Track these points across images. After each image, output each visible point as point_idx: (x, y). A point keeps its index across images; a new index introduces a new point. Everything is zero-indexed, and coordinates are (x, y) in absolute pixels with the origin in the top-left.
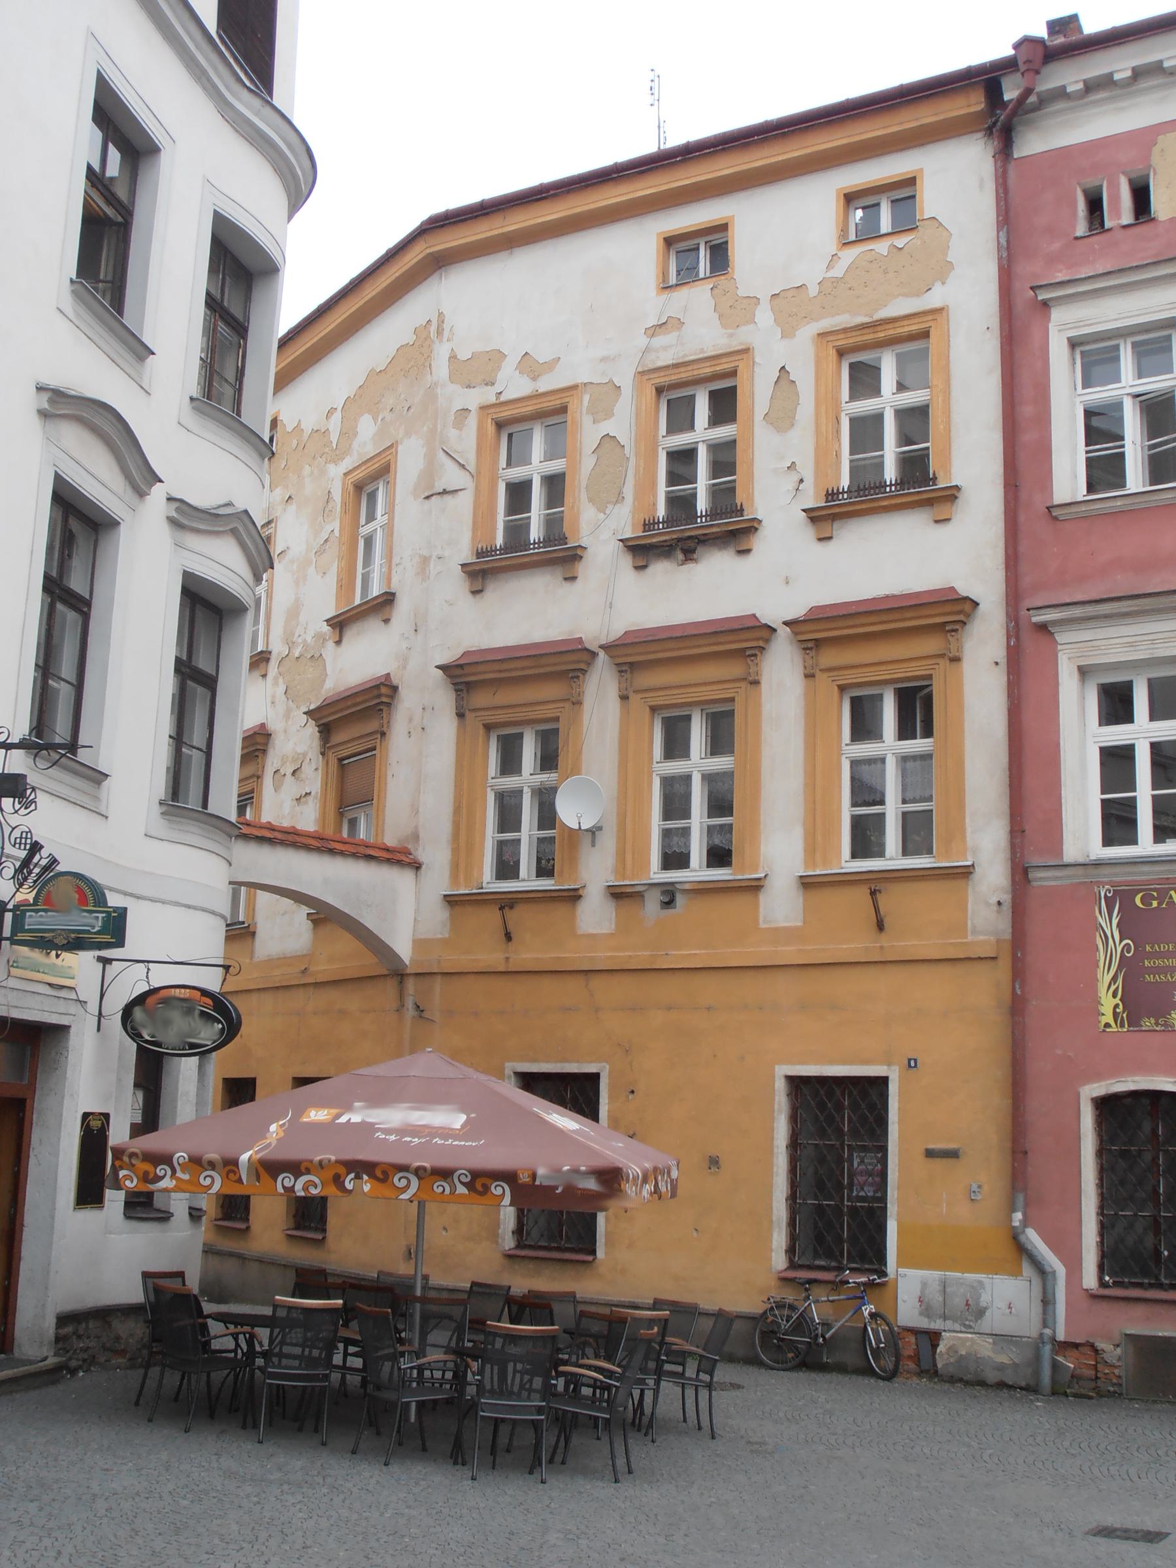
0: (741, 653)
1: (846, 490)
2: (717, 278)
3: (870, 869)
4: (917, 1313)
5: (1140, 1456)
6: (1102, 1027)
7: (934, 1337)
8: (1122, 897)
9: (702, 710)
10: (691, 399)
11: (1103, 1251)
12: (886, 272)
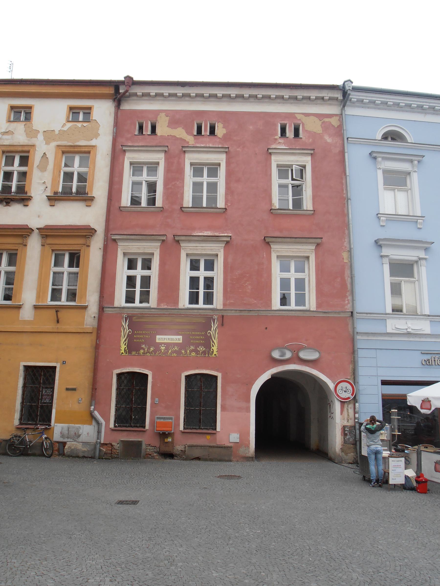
0: (21, 236)
1: (60, 192)
2: (27, 122)
3: (56, 304)
4: (60, 437)
5: (127, 476)
6: (121, 354)
7: (64, 444)
8: (130, 318)
9: (7, 252)
10: (14, 158)
11: (116, 417)
12: (80, 132)
